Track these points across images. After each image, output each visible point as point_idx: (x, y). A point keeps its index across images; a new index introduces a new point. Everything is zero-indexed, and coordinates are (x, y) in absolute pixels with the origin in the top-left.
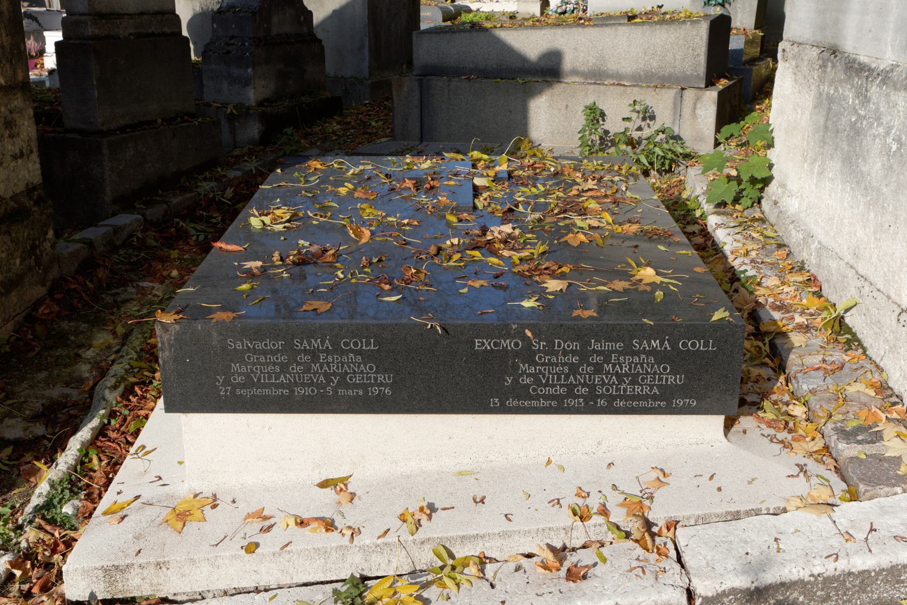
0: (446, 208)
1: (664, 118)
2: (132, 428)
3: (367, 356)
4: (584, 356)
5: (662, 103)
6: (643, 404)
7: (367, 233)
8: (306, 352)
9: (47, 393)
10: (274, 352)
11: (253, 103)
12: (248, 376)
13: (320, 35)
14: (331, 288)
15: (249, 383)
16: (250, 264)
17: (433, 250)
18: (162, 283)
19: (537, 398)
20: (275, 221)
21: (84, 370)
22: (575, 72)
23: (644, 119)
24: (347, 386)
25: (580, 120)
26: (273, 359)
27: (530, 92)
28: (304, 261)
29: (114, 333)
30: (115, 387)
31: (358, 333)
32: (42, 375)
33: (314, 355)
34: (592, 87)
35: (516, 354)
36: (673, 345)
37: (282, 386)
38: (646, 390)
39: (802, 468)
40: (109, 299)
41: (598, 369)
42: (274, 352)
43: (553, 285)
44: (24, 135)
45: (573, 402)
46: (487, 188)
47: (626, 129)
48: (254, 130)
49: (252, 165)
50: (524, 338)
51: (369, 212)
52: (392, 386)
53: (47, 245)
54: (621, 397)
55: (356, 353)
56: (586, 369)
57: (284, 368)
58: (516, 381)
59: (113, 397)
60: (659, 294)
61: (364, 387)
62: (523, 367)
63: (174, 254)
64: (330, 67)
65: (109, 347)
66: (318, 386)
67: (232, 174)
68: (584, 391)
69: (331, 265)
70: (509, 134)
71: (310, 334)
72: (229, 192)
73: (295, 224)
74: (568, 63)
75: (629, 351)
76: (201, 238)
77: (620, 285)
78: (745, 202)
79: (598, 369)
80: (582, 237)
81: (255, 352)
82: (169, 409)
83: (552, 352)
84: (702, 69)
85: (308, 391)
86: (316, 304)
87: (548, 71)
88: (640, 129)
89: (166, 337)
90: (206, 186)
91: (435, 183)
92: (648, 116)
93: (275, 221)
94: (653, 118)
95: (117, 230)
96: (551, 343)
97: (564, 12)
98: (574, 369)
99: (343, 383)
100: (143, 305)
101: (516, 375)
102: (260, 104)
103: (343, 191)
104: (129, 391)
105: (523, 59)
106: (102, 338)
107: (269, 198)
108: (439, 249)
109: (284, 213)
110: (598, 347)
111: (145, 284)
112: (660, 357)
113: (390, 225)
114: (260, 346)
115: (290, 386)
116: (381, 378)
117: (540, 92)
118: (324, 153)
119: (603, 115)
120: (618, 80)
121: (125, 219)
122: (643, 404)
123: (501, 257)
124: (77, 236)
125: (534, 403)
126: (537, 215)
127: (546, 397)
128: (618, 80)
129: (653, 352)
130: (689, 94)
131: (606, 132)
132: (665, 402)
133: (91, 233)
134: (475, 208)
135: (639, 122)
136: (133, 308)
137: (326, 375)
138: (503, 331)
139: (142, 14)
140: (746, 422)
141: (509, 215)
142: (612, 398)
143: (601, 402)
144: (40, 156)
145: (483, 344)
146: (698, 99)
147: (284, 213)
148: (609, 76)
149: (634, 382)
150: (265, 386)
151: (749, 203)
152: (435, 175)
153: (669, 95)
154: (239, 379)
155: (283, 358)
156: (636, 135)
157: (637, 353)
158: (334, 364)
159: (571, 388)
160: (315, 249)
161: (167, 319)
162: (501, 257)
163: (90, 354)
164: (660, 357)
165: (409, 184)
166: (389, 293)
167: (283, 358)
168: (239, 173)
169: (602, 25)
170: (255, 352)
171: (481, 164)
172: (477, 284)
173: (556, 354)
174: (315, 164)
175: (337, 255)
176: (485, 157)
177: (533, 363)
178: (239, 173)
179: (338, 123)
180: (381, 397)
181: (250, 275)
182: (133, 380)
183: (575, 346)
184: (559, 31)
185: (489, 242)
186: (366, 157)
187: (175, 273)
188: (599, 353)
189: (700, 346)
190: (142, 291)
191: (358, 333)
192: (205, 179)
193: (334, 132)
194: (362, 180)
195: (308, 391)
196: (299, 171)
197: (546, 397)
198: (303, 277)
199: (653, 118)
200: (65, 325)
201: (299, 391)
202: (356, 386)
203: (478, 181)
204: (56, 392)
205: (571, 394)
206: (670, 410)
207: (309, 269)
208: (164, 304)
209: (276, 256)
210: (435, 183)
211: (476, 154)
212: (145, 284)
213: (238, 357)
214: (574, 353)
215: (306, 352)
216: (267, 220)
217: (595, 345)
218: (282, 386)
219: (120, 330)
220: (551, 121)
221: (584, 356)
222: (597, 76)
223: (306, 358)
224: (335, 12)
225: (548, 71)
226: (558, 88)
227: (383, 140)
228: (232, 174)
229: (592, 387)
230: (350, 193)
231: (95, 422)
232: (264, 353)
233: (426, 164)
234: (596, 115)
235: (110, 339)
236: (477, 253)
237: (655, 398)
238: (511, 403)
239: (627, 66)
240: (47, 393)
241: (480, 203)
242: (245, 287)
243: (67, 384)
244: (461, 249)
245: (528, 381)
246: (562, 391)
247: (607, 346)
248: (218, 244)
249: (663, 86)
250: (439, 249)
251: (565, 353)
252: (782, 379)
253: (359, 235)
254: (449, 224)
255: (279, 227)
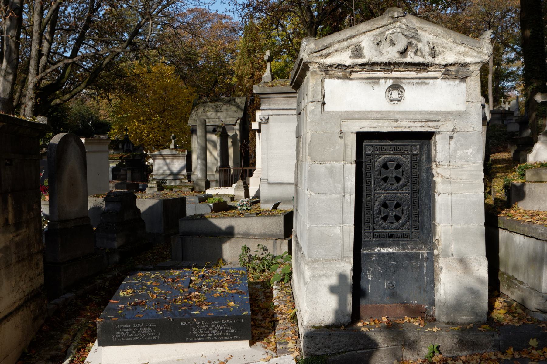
0: (180, 287)
1: (271, 251)
2: (81, 360)
3: (153, 328)
4: (210, 325)
5: (269, 244)
6: (226, 338)
7: (155, 296)
8: (136, 327)
9: (50, 353)
10: (128, 328)
11: (116, 247)
12: (121, 335)
13: (143, 217)
14: (144, 311)
15: (121, 337)
16: (120, 306)
17: (173, 300)
18: (84, 318)
19: (198, 337)
20: (127, 293)
21: (61, 346)
22: (239, 234)
23: (264, 251)
24: (148, 337)
25: (240, 251)
26: (127, 330)
27: (223, 242)
28: (136, 304)
29: (70, 335)
30: (74, 349)
31: (150, 321)
32: (48, 348)
33: (139, 328)
34: (244, 239)
35: (192, 326)
36: (233, 321)
37: (130, 337)
38: (227, 334)
39: (267, 352)
40: (66, 324)
41: (214, 329)
42: (128, 328)
43: (205, 308)
44: (40, 268)
45: (208, 338)
46: (195, 280)
47: (256, 255)
48: (117, 258)
49: (116, 272)
50: (194, 321)
51: (156, 290)
52: (159, 336)
53: (45, 305)
54: (221, 336)
55: (150, 327)
56: (210, 329)
57: (131, 332)
58: (192, 333)
59: (74, 352)
60: (232, 309)
61: (152, 336)
62: (194, 329)
63: (88, 307)
64: (148, 230)
65: (68, 339)
66: (140, 337)
67: (108, 276)
68: (211, 335)
69: (144, 305)
70: (216, 258)
71: (138, 322)
72: (107, 283)
73: (134, 294)
74: (236, 231)
75: (221, 323)
76: (97, 301)
77: (223, 307)
78: (285, 281)
79: (214, 329)
80: (218, 295)
81: (123, 328)
82: (99, 345)
83: (201, 324)
84: (283, 232)
85: (137, 338)
86: (139, 315)
87: (229, 233)
88: (262, 254)
89: (99, 325)
90: (99, 281)
91: (179, 279)
92: (265, 249)
93: (127, 293)
94: (267, 250)
95: (67, 299)
96: (201, 322)
97: (243, 205)
98: (207, 329)
99: (147, 336)
100: (78, 326)
101: (192, 332)
102: (119, 248)
103: (149, 283)
104: (79, 350)
105: (220, 229)
106: (66, 336)
107: (125, 286)
108: (176, 300)
109: (130, 291)
110: (213, 323)
111: (78, 318)
112: (230, 325)
113: (163, 293)
114: (124, 326)
115: (132, 337)
116: (156, 334)
117: (226, 242)
118: (143, 270)
119: (249, 249)
120: (254, 237)
121: (69, 295)
122: (226, 338)
123: (193, 301)
124: (53, 302)
125: (198, 339)
126: (207, 289)
127: (201, 337)
128: (254, 237)
129: (228, 324)
130: (278, 241)
131: (251, 256)
132: (232, 337)
133: (57, 301)
134: (189, 287)
135: (262, 251)
136: (75, 326)
137: (142, 334)
138: (188, 320)
139: (76, 219)
140: (258, 344)
141: (199, 289)
142: (218, 337)
143: (215, 338)
144: (44, 274)
145: (183, 323)
146: (281, 243)
147: (130, 291)
148: (251, 235)
149: (223, 332)
150: (125, 338)
151: (287, 281)
152: (179, 276)
153: (271, 242)
154: (119, 336)
155: (131, 330)
156: (261, 256)
157: (224, 324)
158: (144, 330)
159: (207, 334)
160: (139, 301)
161: (100, 320)
162: (193, 301)
163: (62, 341)
164: (230, 325)
165: (170, 280)
166: (160, 311)
167: (131, 330)
168: (111, 276)
169: (247, 217)
170: (123, 328)
171: (195, 272)
172: (184, 308)
173: (202, 325)
174: (140, 274)
175: (146, 303)
176: (197, 269)
177: (197, 328)
178: (111, 276)
179: (151, 253)
180: (156, 339)
181: (121, 309)
182: (80, 347)
183: (207, 323)
184: (232, 219)
185: (191, 297)
186: (410, 66)
187: (89, 314)
188: (214, 324)
189: (240, 321)
190: (523, 65)
191: (150, 321)
192: (98, 279)
193: (149, 257)
194: (157, 279)
195: (137, 338)
196: (135, 276)
197: (201, 337)
198: (136, 309)
199: (267, 250)
200: (52, 333)
201: (135, 338)
202: (150, 336)
203: (192, 278)
204: (53, 353)
205: (207, 336)
206: (234, 339)
207: (137, 307)
208: (99, 316)
209: (128, 303)
210: (179, 279)
211: (194, 269)
212: (78, 318)
213: (118, 329)
214: (207, 325)
215: (136, 327)
216: (125, 293)
217: (212, 322)
218: (130, 337)
219: (72, 333)
220: (230, 251)
221: (210, 325)
222: (246, 235)
223: (136, 329)
224: (150, 207)
225: (229, 233)
226: (233, 240)
227: (168, 260)
228: (108, 276)
229: (213, 334)
230: (151, 283)
231: (70, 359)
232: (125, 328)
233: (177, 273)
234: (247, 249)
235: (69, 336)
236: (186, 300)
237: (229, 336)
238: (191, 339)
239: (257, 232)
240: (50, 353)
241: (191, 286)
242: (120, 312)
243: (56, 350)
244: (182, 300)
245: (196, 333)
246: (205, 335)
247: (216, 322)
248: (111, 301)
249: (270, 239)
250: (176, 300)
251: (205, 325)
252: (273, 332)
253: (153, 297)
254: (180, 292)
255: (129, 295)
